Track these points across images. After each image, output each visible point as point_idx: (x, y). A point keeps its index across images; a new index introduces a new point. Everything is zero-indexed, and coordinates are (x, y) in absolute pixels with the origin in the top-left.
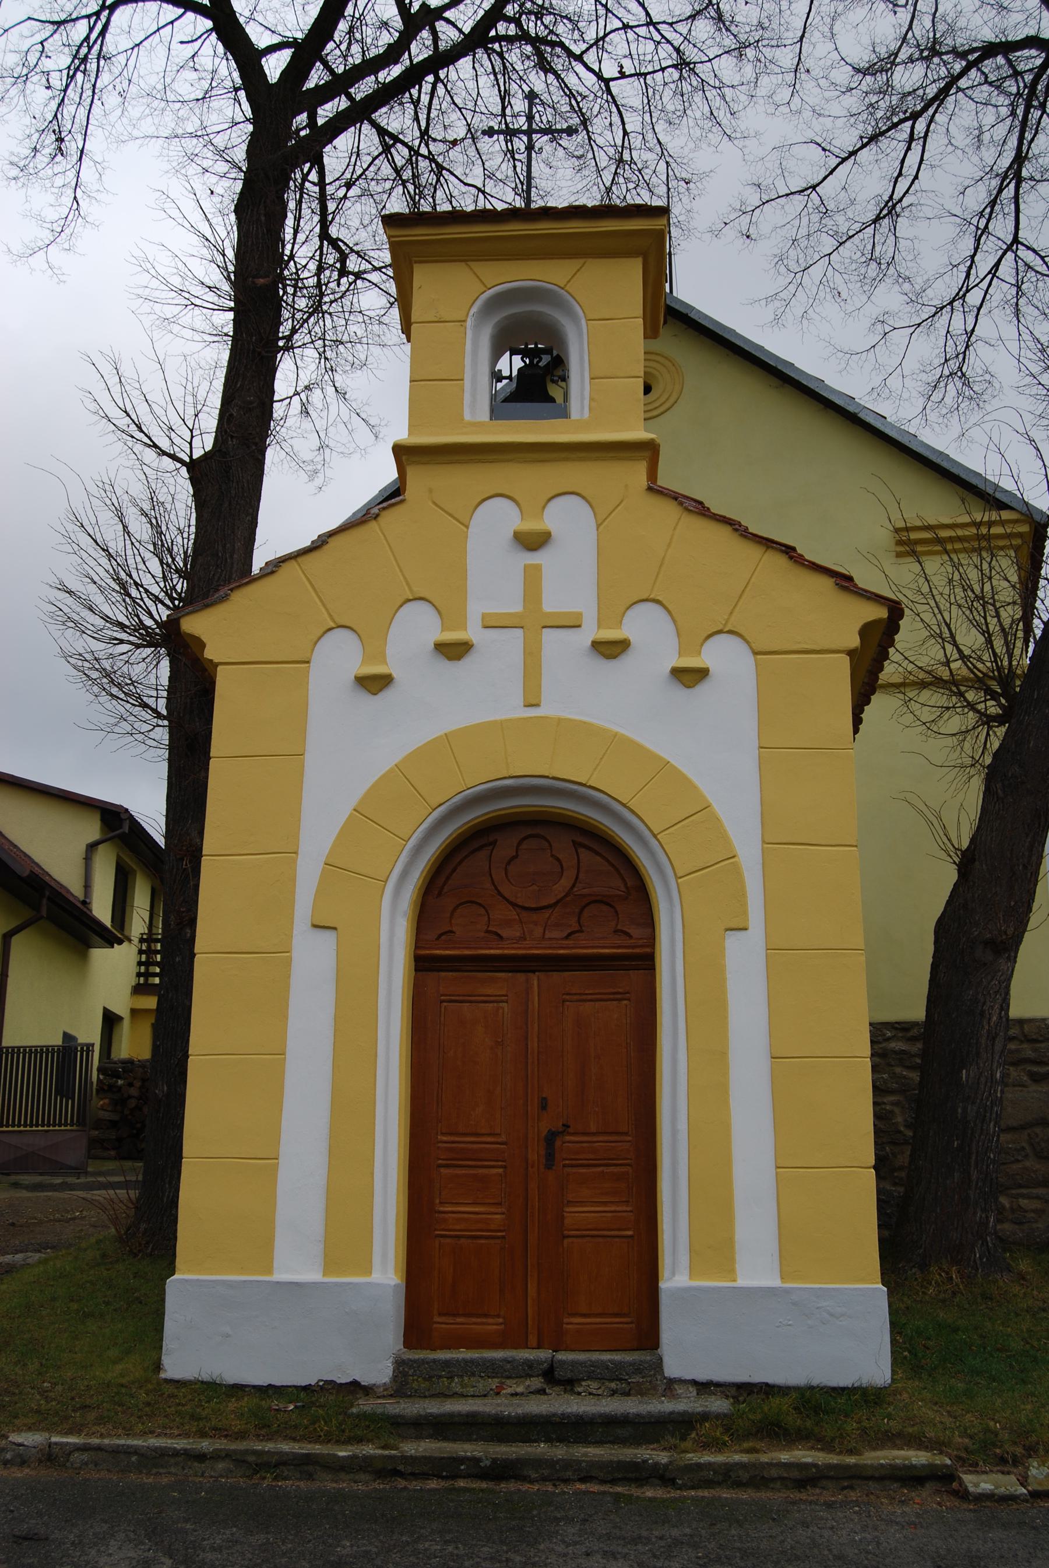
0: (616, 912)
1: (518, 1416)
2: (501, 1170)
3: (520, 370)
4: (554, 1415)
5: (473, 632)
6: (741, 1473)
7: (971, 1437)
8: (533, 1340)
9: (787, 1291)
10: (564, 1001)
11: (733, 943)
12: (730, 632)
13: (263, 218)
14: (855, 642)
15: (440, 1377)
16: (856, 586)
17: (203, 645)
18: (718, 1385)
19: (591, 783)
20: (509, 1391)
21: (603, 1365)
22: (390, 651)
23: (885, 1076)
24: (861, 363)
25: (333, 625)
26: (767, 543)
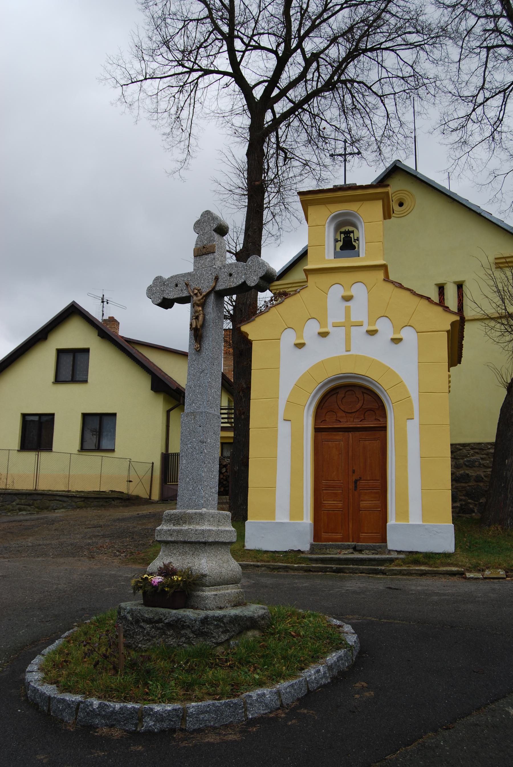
0: (375, 413)
1: (344, 558)
2: (341, 491)
3: (343, 238)
4: (355, 558)
5: (329, 328)
6: (404, 572)
7: (472, 565)
8: (351, 540)
9: (424, 525)
10: (360, 441)
11: (409, 422)
12: (409, 326)
13: (256, 158)
14: (449, 328)
15: (323, 549)
16: (450, 310)
17: (248, 335)
18: (403, 552)
19: (366, 375)
20: (343, 553)
21: (370, 546)
22: (304, 335)
23: (488, 462)
24: (486, 188)
25: (287, 327)
26: (421, 296)
